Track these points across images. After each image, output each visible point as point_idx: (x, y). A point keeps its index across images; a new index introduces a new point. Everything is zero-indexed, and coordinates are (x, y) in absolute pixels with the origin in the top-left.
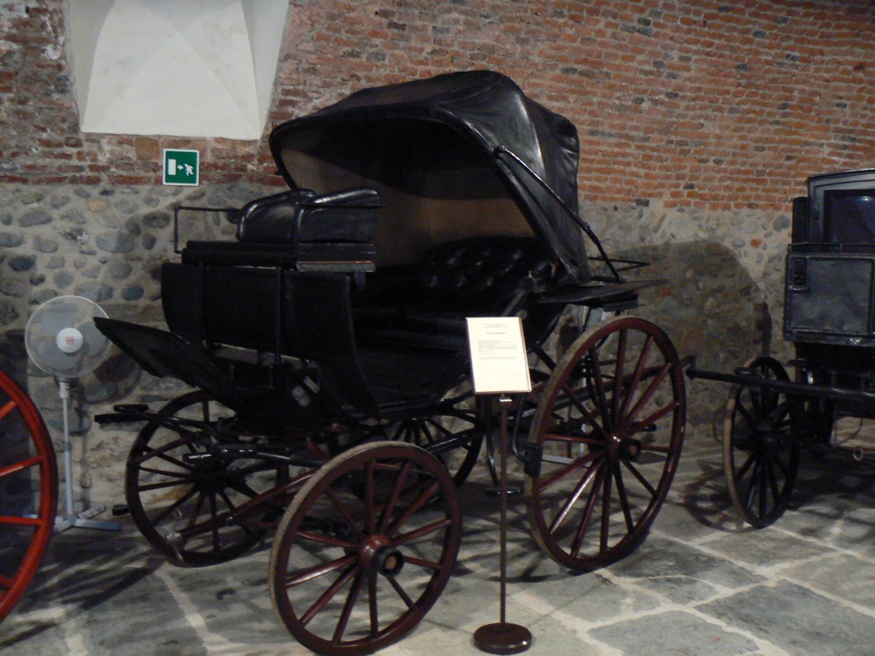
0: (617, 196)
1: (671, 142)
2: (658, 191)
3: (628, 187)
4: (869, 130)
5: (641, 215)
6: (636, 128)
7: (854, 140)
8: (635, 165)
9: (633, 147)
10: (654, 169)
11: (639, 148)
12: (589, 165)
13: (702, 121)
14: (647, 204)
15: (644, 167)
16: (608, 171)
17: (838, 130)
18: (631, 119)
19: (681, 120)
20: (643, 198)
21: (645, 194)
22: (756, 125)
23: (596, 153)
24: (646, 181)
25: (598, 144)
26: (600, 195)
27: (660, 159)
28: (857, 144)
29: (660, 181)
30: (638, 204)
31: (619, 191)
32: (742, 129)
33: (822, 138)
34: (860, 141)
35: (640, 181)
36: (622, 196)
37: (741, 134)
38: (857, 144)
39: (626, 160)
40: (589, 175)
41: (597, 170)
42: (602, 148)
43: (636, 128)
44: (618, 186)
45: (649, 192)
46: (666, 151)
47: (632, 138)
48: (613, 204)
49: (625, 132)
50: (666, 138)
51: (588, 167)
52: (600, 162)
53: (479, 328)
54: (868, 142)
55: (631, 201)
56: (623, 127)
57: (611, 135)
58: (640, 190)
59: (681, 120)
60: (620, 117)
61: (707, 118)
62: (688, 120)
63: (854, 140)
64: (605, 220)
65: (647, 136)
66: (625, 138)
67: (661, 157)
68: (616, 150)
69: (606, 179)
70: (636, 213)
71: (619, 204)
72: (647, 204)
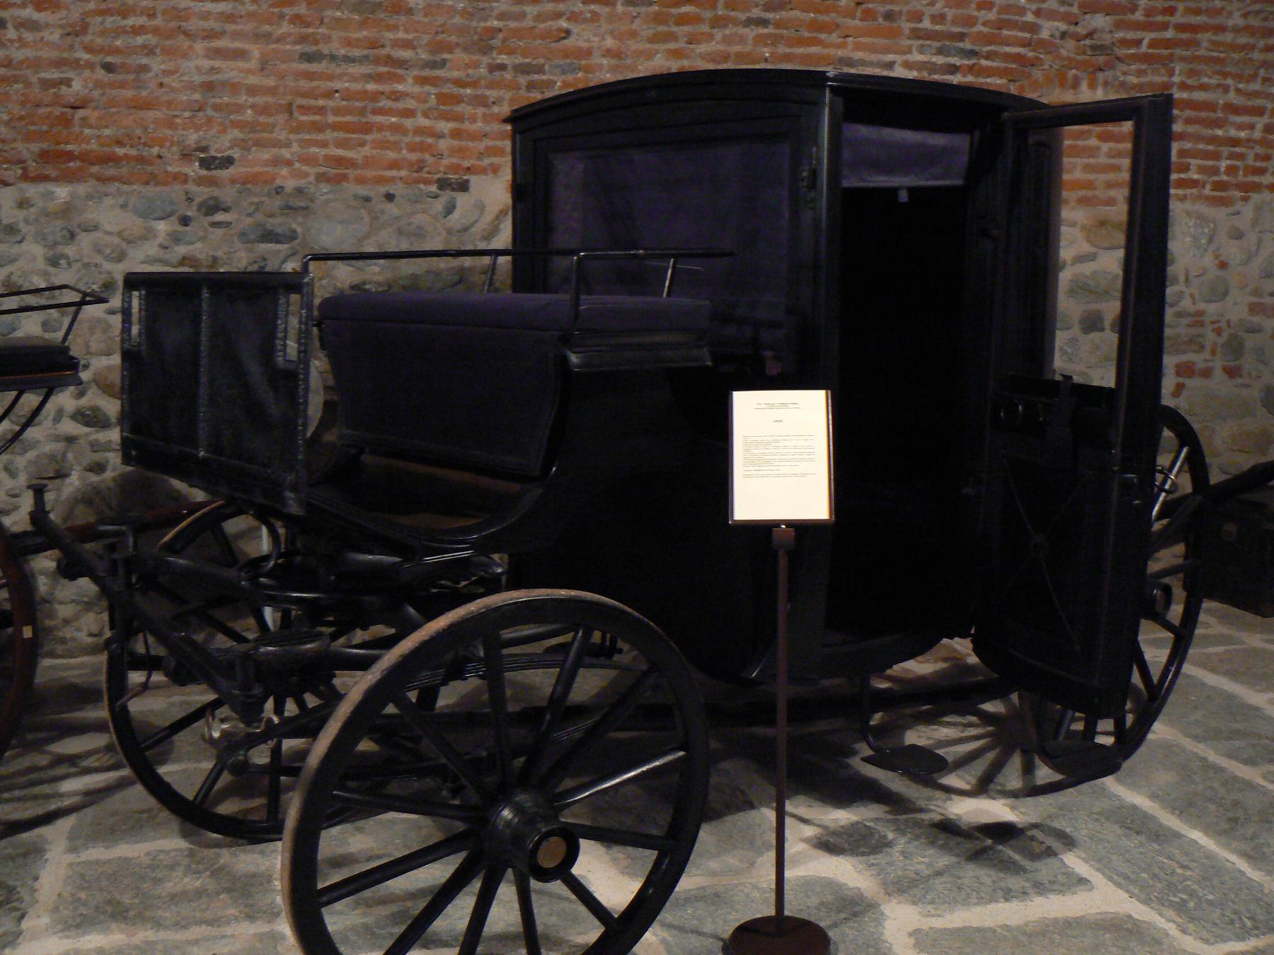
0: (393, 173)
1: (502, 67)
2: (486, 162)
3: (414, 157)
4: (1005, 32)
5: (450, 209)
6: (407, 45)
7: (973, 53)
8: (426, 115)
9: (410, 81)
10: (473, 120)
11: (423, 81)
12: (317, 118)
13: (564, 24)
14: (463, 187)
15: (445, 117)
16: (366, 128)
17: (916, 34)
18: (395, 28)
19: (513, 24)
20: (453, 177)
21: (456, 168)
22: (705, 28)
23: (329, 94)
24: (456, 143)
25: (331, 78)
26: (351, 173)
27: (481, 101)
28: (984, 63)
29: (488, 142)
30: (441, 188)
31: (394, 165)
32: (672, 37)
33: (888, 50)
34: (988, 56)
35: (443, 144)
36: (403, 173)
37: (672, 46)
38: (984, 63)
39: (400, 105)
40: (320, 137)
41: (336, 127)
42: (337, 85)
43: (407, 45)
44: (391, 155)
45: (466, 164)
46: (492, 85)
47: (402, 63)
48: (383, 189)
49: (384, 52)
50: (485, 60)
51: (314, 123)
52: (337, 111)
53: (813, 502)
54: (1008, 57)
55: (427, 182)
56: (374, 45)
57: (348, 60)
58: (445, 162)
59: (513, 24)
60: (363, 24)
61: (574, 17)
62: (528, 23)
63: (973, 53)
64: (367, 219)
65: (438, 58)
66: (386, 64)
67: (484, 96)
68: (371, 87)
69: (362, 144)
70: (439, 206)
71: (398, 189)
72: (463, 187)
